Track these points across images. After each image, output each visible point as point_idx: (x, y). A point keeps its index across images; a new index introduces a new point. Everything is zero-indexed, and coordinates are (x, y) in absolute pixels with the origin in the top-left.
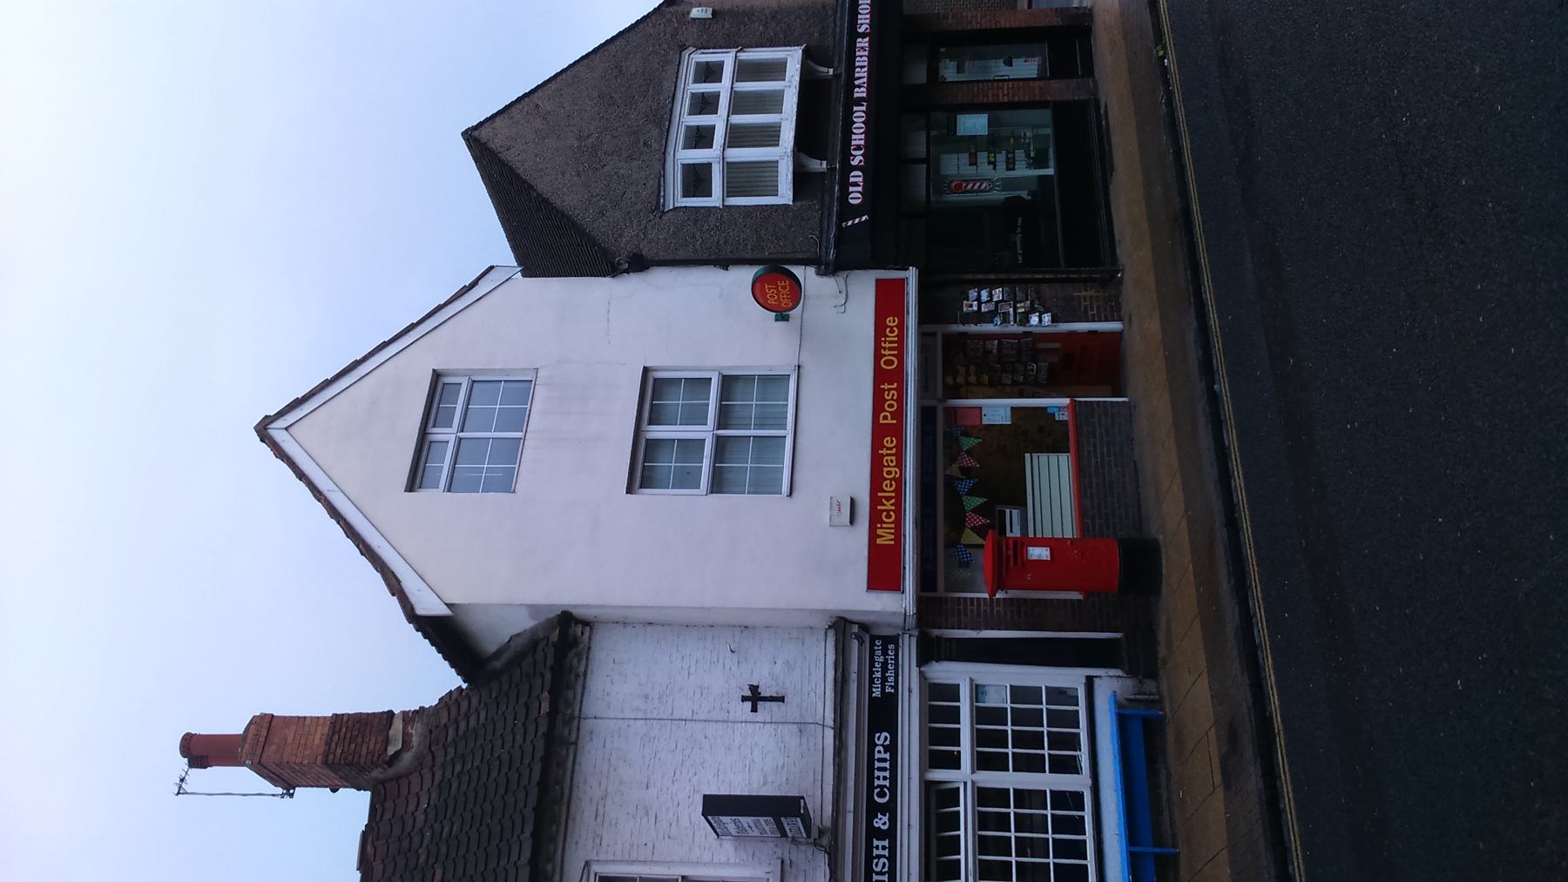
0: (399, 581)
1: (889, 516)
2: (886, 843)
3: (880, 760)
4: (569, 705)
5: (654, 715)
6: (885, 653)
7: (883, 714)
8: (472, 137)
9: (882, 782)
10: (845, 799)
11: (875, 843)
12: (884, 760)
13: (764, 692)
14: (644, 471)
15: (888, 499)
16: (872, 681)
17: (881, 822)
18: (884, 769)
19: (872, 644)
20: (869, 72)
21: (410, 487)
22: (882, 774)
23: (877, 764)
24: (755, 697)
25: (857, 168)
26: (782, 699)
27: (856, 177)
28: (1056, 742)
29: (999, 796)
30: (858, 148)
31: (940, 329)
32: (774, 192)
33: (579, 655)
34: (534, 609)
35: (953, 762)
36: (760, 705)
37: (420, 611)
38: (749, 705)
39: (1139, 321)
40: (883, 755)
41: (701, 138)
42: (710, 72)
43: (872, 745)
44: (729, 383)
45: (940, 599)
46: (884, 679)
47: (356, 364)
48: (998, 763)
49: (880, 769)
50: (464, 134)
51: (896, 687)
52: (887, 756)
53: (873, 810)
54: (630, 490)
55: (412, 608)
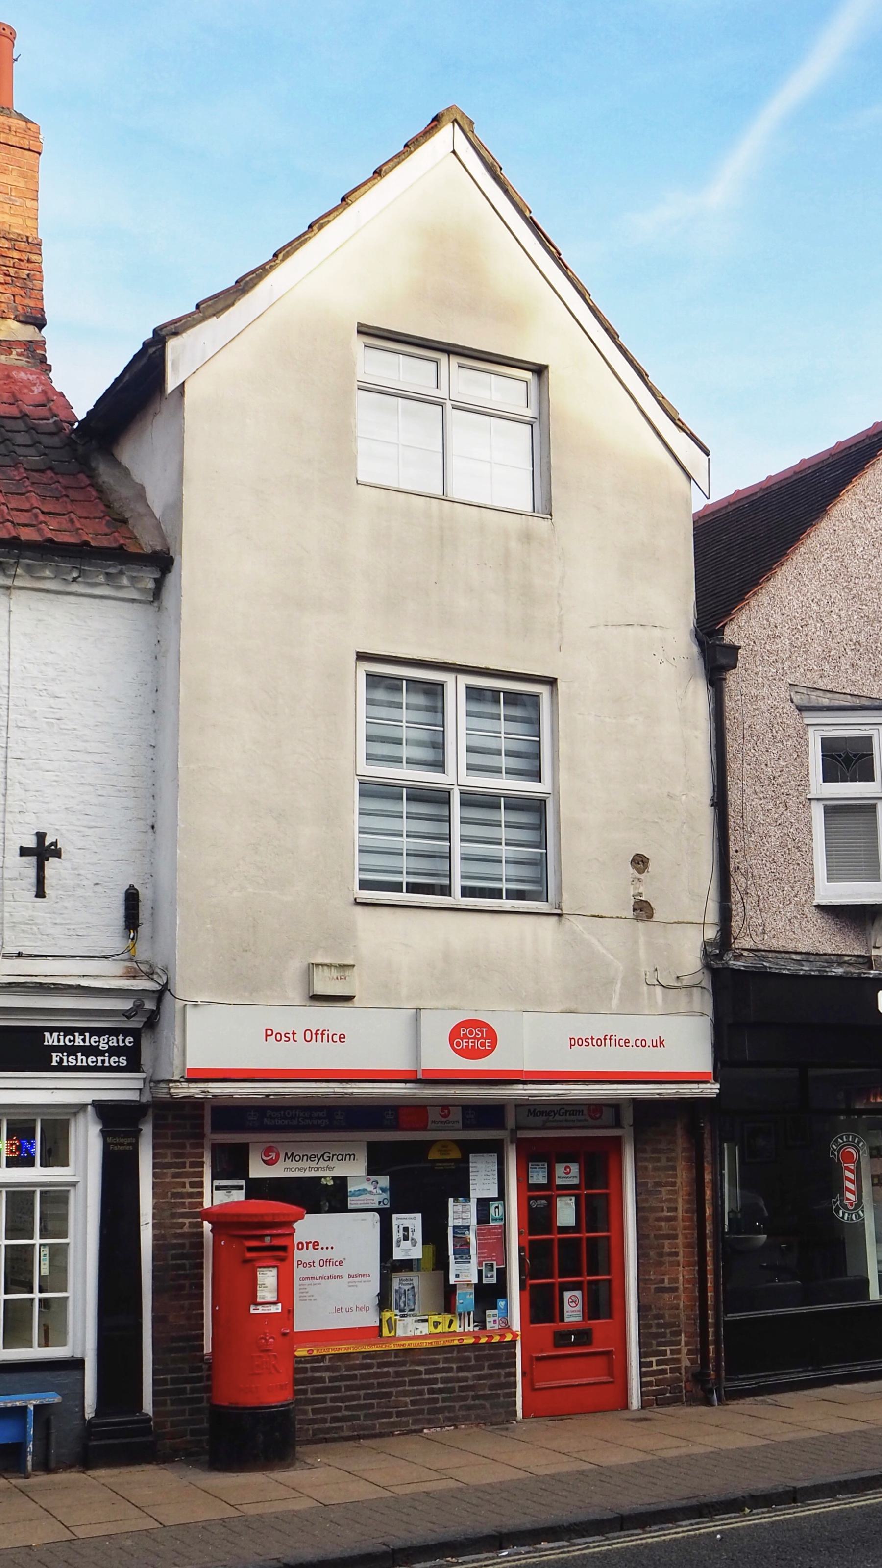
1: (70, 1041)
6: (114, 1051)
13: (52, 866)
14: (401, 681)
15: (84, 1040)
16: (69, 1031)
19: (126, 1032)
24: (42, 852)
26: (40, 893)
31: (627, 1134)
34: (176, 507)
37: (172, 346)
39: (650, 1446)
44: (536, 807)
45: (202, 1136)
46: (72, 1050)
51: (60, 1068)
54: (362, 657)
55: (176, 334)
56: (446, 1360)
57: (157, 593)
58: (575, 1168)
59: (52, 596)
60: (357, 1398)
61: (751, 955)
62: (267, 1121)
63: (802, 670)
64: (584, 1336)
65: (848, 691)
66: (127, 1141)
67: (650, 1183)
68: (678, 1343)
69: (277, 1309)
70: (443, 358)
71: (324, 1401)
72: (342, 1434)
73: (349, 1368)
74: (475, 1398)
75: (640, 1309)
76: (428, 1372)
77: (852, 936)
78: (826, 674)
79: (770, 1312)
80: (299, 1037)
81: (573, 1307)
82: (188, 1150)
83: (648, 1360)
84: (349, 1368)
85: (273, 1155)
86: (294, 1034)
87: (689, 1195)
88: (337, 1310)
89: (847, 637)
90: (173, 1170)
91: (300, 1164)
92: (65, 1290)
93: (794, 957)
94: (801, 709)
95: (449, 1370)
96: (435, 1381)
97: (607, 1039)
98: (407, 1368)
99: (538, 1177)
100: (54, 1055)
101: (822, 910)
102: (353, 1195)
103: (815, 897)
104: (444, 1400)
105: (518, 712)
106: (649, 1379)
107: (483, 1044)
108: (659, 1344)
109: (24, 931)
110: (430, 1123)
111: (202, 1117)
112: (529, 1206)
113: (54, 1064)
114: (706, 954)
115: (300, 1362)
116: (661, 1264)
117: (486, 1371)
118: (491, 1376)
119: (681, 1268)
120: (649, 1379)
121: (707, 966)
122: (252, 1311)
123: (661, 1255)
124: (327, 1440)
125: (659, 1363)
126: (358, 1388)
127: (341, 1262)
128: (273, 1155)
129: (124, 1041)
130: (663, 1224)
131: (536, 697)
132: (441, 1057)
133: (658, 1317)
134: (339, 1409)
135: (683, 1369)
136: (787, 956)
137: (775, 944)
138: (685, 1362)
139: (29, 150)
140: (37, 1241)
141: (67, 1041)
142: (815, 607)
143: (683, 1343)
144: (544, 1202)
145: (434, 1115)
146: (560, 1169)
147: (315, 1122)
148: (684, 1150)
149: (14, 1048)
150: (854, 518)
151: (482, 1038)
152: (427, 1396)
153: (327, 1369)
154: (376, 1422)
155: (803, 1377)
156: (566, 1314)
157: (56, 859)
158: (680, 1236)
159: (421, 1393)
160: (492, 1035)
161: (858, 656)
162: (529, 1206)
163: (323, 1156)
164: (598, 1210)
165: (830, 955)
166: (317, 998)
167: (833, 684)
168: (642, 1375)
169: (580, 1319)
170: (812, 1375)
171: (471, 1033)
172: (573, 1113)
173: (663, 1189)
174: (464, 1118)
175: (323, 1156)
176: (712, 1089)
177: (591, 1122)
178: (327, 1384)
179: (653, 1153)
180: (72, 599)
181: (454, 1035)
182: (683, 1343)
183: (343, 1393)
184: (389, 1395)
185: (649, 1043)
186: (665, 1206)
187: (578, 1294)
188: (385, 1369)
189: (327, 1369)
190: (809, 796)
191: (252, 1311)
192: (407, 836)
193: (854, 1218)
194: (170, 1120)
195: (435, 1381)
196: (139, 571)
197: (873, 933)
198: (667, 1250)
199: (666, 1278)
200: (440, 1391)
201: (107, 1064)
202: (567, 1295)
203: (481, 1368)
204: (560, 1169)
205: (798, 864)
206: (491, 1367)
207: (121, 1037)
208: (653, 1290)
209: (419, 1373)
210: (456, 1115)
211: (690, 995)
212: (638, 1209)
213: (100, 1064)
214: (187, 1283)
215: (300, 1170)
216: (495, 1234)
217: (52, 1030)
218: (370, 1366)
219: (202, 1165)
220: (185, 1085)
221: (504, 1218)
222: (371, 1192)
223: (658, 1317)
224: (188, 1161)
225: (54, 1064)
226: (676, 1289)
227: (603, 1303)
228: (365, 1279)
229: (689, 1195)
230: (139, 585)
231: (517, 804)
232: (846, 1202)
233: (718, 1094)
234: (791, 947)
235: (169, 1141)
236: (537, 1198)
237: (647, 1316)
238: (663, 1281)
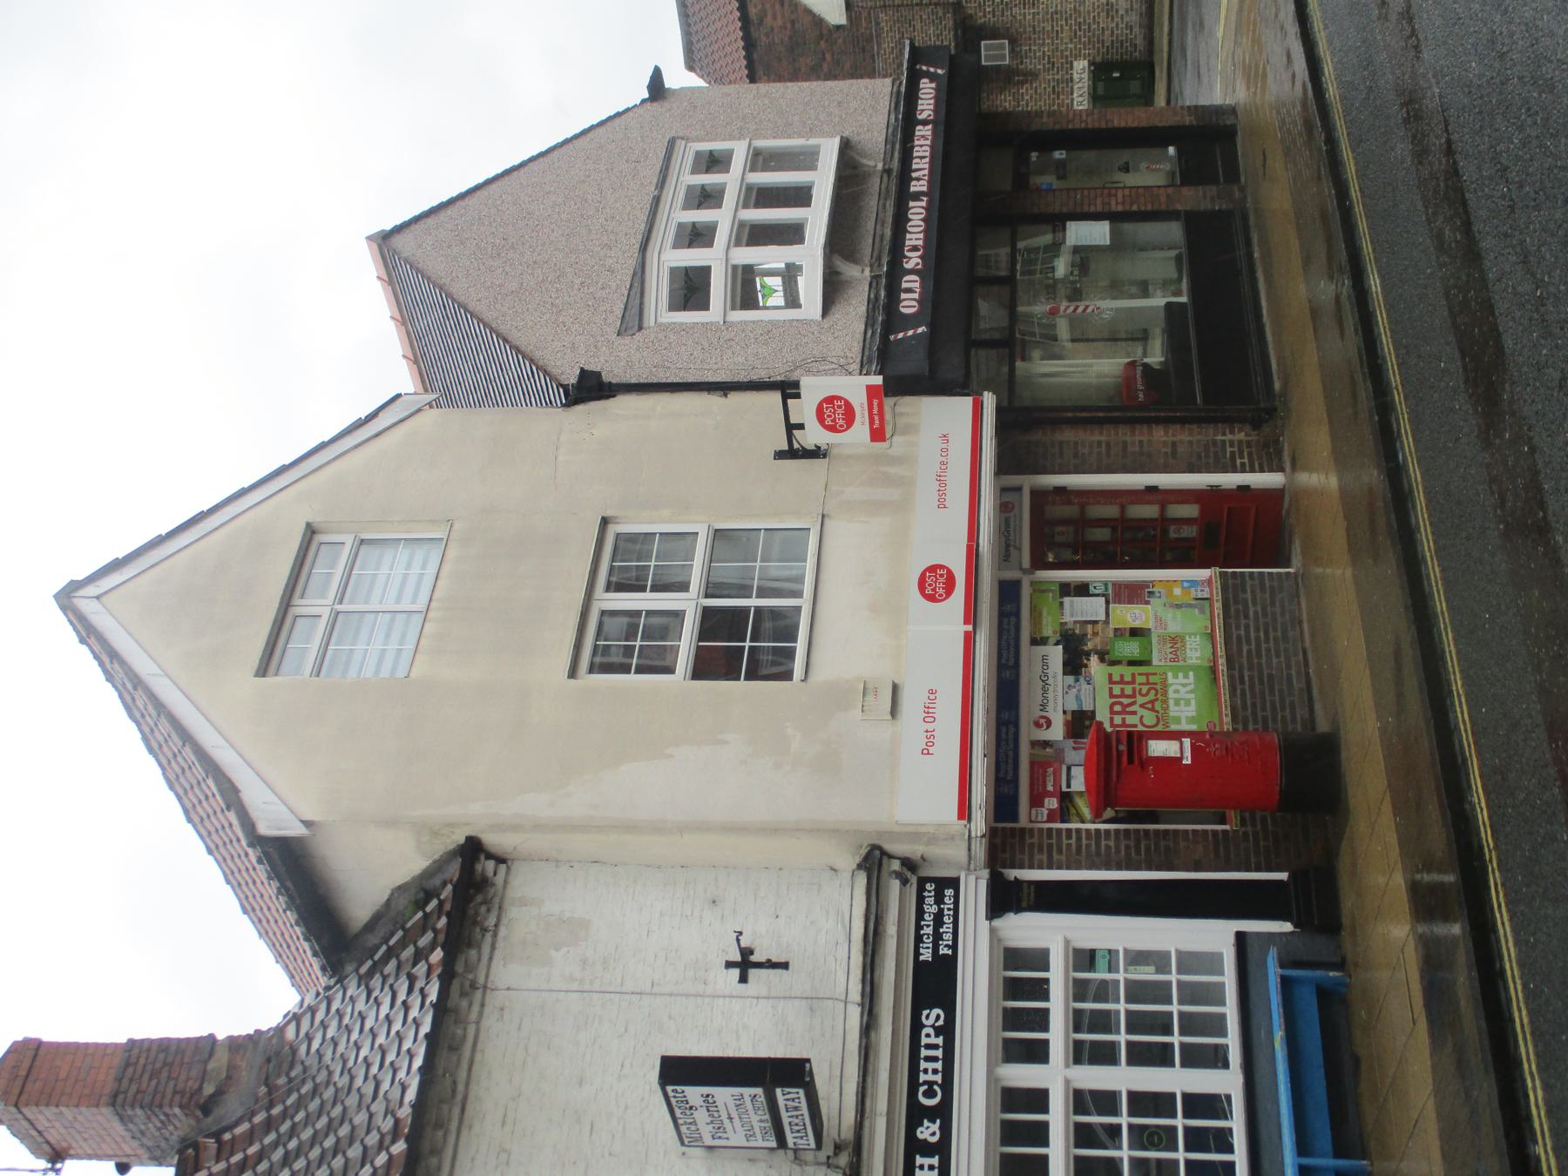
0: (236, 791)
2: (935, 1161)
3: (928, 1046)
4: (470, 968)
5: (596, 987)
6: (939, 900)
7: (935, 983)
8: (384, 241)
9: (930, 1077)
10: (874, 1097)
11: (919, 1160)
12: (935, 1047)
16: (919, 939)
17: (928, 1132)
18: (935, 1059)
20: (931, 163)
21: (262, 671)
22: (930, 1066)
25: (912, 272)
26: (784, 966)
27: (911, 282)
28: (1190, 1024)
29: (1105, 1101)
30: (915, 248)
31: (1029, 481)
33: (487, 902)
35: (1036, 1053)
36: (753, 973)
37: (264, 829)
38: (736, 972)
40: (933, 1040)
41: (698, 236)
42: (714, 162)
43: (917, 1026)
45: (1023, 830)
46: (937, 936)
48: (1104, 1055)
49: (928, 1059)
50: (57, 597)
51: (954, 947)
52: (940, 1041)
53: (916, 1114)
54: (573, 674)
56: (1238, 628)
57: (501, 860)
62: (1011, 663)
66: (1026, 891)
69: (1187, 742)
70: (294, 611)
80: (930, 727)
92: (1173, 1095)
96: (1258, 638)
97: (940, 479)
98: (1245, 660)
104: (1275, 630)
111: (1004, 829)
117: (1249, 595)
125: (1242, 457)
133: (1199, 457)
134: (1278, 656)
138: (1242, 436)
141: (928, 942)
159: (1268, 650)
160: (933, 569)
176: (989, 400)
177: (1016, 510)
184: (1270, 677)
186: (1096, 450)
200: (1266, 633)
203: (1245, 600)
206: (1244, 591)
209: (1249, 651)
211: (902, 414)
212: (1099, 471)
214: (1163, 843)
217: (917, 954)
218: (1243, 691)
223: (1199, 457)
226: (1174, 444)
234: (861, 337)
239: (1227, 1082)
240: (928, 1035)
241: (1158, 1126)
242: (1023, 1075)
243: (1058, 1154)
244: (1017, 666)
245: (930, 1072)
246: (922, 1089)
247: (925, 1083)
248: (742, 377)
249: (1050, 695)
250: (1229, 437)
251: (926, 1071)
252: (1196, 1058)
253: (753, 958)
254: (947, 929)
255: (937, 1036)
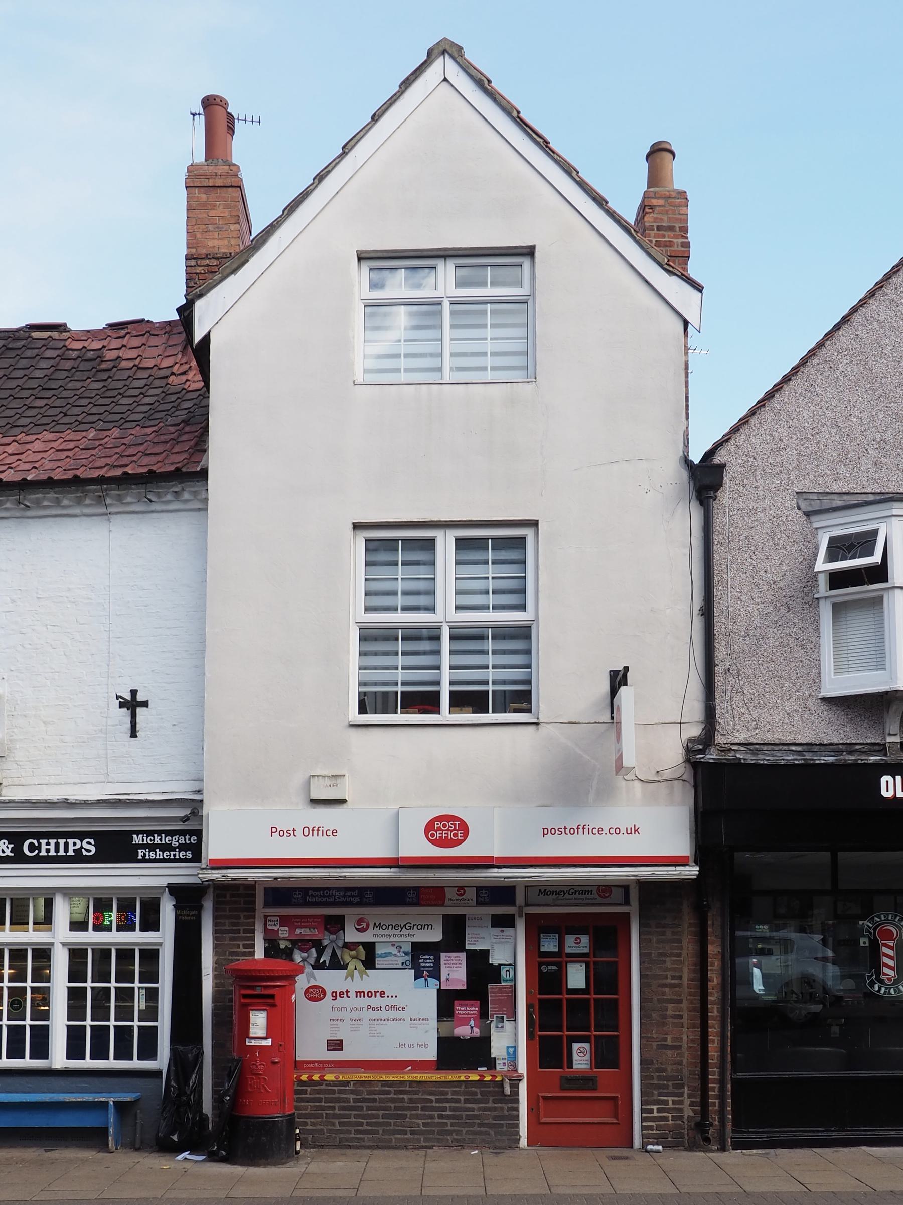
3: (66, 845)
6: (182, 847)
7: (115, 846)
12: (66, 850)
14: (395, 545)
15: (161, 840)
16: (150, 833)
18: (57, 850)
21: (362, 257)
23: (62, 842)
24: (132, 704)
26: (134, 733)
29: (42, 972)
31: (633, 910)
32: (839, 669)
38: (140, 698)
40: (71, 848)
43: (81, 836)
45: (254, 910)
46: (152, 847)
47: (544, 145)
49: (57, 846)
51: (144, 860)
58: (585, 940)
59: (141, 516)
60: (377, 1117)
61: (742, 748)
63: (812, 477)
64: (585, 1081)
65: (869, 490)
67: (654, 954)
68: (682, 1095)
71: (349, 1116)
72: (363, 1144)
73: (370, 1093)
74: (480, 1125)
75: (642, 1062)
76: (437, 1101)
77: (865, 725)
78: (841, 477)
79: (787, 1074)
81: (581, 1057)
82: (242, 920)
83: (649, 1107)
84: (370, 1093)
85: (364, 925)
86: (294, 830)
87: (695, 965)
88: (401, 1046)
89: (870, 437)
90: (231, 935)
91: (386, 932)
93: (793, 748)
94: (808, 514)
95: (458, 1101)
96: (445, 1109)
98: (420, 1096)
99: (549, 945)
100: (140, 851)
101: (836, 705)
102: (380, 957)
103: (822, 690)
105: (504, 555)
106: (649, 1124)
107: (456, 835)
108: (660, 1094)
109: (123, 763)
110: (447, 899)
112: (540, 971)
113: (140, 857)
114: (688, 750)
115: (330, 1085)
116: (664, 1024)
117: (490, 1104)
118: (495, 1109)
119: (685, 1030)
120: (649, 1124)
121: (687, 760)
122: (247, 1044)
123: (664, 1017)
124: (350, 1147)
126: (378, 1109)
127: (403, 1008)
128: (364, 925)
129: (189, 840)
130: (667, 989)
131: (523, 539)
132: (418, 846)
133: (659, 1070)
134: (362, 1124)
135: (686, 1117)
136: (785, 747)
137: (769, 737)
138: (688, 1112)
139: (231, 186)
140: (137, 984)
142: (829, 414)
143: (686, 1095)
144: (554, 967)
145: (450, 894)
146: (570, 940)
147: (348, 899)
148: (690, 925)
149: (23, 844)
150: (882, 319)
151: (455, 830)
152: (437, 1120)
153: (352, 1092)
154: (392, 1137)
155: (823, 1135)
156: (574, 1063)
157: (145, 709)
158: (685, 1001)
160: (464, 828)
161: (883, 452)
162: (540, 971)
163: (405, 926)
164: (608, 978)
165: (837, 744)
166: (315, 802)
167: (851, 485)
168: (643, 1119)
169: (588, 1067)
170: (843, 1135)
171: (444, 826)
172: (583, 892)
173: (668, 959)
174: (478, 896)
175: (405, 926)
176: (692, 871)
177: (600, 900)
178: (352, 1104)
179: (657, 927)
180: (154, 515)
181: (429, 827)
182: (686, 1095)
183: (365, 1111)
185: (623, 831)
187: (587, 1046)
188: (401, 1096)
189: (352, 1092)
190: (816, 596)
191: (247, 1044)
192: (402, 669)
193: (892, 991)
194: (228, 898)
195: (445, 1109)
196: (193, 487)
197: (888, 721)
198: (670, 1012)
199: (669, 1038)
200: (449, 1117)
201: (177, 857)
202: (576, 1046)
204: (570, 940)
205: (801, 661)
207: (187, 837)
208: (655, 1047)
209: (431, 1101)
210: (471, 894)
212: (642, 976)
213: (172, 857)
215: (386, 936)
216: (506, 992)
217: (138, 833)
218: (389, 1092)
219: (253, 931)
220: (210, 871)
221: (514, 979)
222: (395, 955)
223: (659, 1070)
224: (242, 928)
225: (140, 857)
226: (679, 1048)
227: (611, 1054)
228: (424, 1022)
229: (695, 965)
230: (199, 497)
231: (504, 633)
232: (882, 977)
233: (698, 876)
234: (789, 738)
235: (227, 913)
236: (548, 964)
237: (648, 1069)
238: (665, 1040)
239: (58, 1058)
240: (75, 844)
241: (25, 1007)
242: (62, 912)
243: (8, 936)
244: (417, 903)
245: (47, 847)
246: (35, 842)
247: (40, 844)
248: (719, 629)
249: (390, 932)
250: (687, 1102)
251: (48, 844)
252: (75, 1038)
253: (139, 710)
254: (159, 854)
255: (74, 850)
